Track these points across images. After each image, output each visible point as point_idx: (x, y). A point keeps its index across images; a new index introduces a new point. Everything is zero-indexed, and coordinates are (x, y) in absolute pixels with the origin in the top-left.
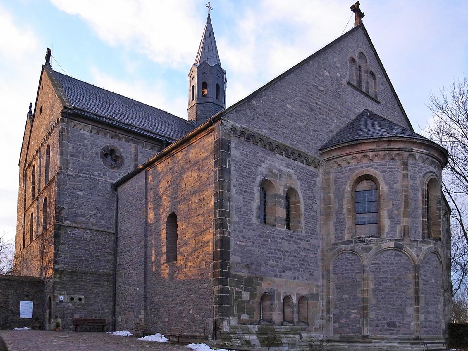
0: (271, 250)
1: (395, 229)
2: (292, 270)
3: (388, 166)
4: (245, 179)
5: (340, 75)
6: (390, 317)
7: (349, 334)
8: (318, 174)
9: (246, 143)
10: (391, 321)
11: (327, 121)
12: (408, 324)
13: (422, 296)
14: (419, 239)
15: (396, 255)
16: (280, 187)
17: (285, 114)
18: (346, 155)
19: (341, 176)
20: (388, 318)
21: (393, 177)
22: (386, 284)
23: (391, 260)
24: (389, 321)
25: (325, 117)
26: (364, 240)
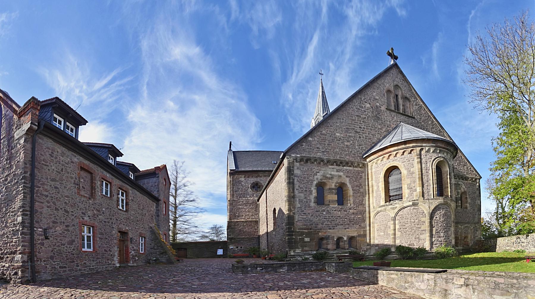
3: (406, 158)
5: (379, 104)
9: (305, 165)
11: (369, 137)
15: (414, 209)
17: (335, 140)
19: (378, 169)
24: (409, 243)
25: (367, 135)
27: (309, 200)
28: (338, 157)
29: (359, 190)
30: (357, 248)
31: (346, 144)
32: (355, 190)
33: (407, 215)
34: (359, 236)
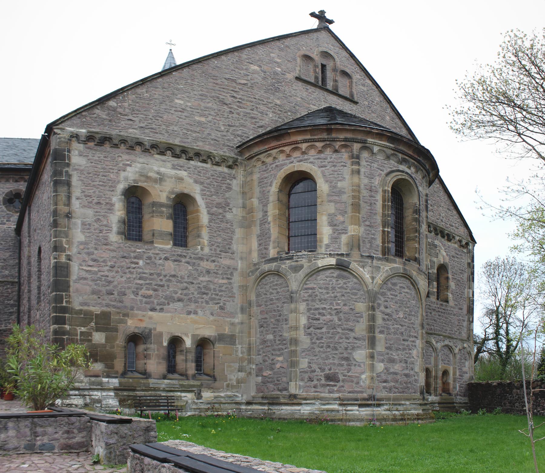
0: (144, 275)
1: (338, 240)
2: (183, 301)
3: (329, 160)
4: (98, 188)
6: (329, 367)
7: (273, 393)
8: (236, 176)
10: (332, 371)
12: (356, 377)
13: (379, 336)
14: (378, 254)
15: (338, 277)
16: (160, 193)
18: (271, 150)
19: (266, 175)
20: (327, 368)
21: (336, 173)
22: (324, 318)
23: (331, 283)
24: (327, 372)
26: (293, 256)
27: (106, 226)
28: (177, 142)
29: (224, 216)
30: (214, 376)
31: (197, 118)
32: (213, 214)
33: (324, 291)
34: (221, 338)
